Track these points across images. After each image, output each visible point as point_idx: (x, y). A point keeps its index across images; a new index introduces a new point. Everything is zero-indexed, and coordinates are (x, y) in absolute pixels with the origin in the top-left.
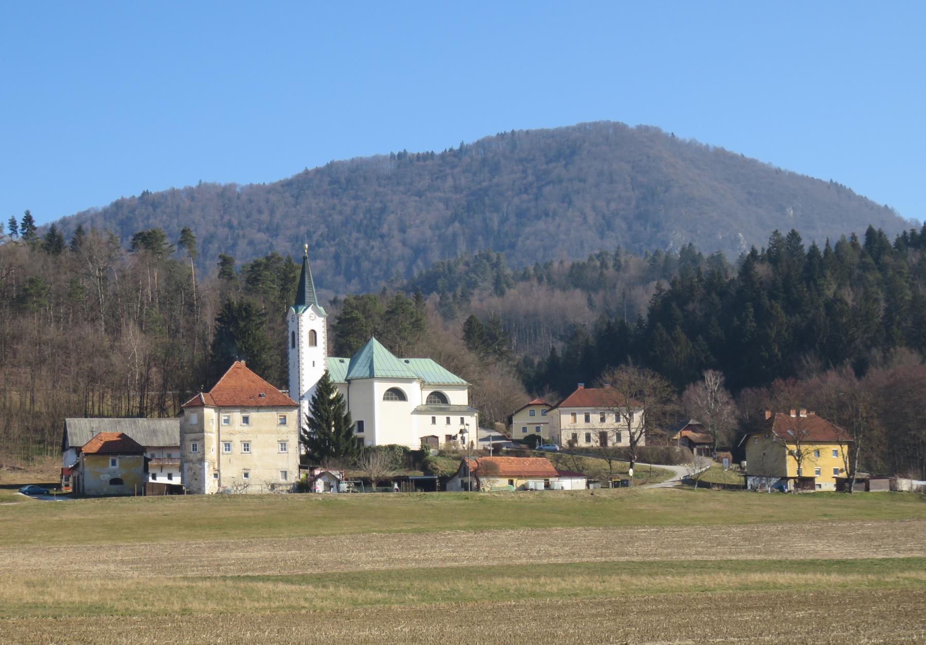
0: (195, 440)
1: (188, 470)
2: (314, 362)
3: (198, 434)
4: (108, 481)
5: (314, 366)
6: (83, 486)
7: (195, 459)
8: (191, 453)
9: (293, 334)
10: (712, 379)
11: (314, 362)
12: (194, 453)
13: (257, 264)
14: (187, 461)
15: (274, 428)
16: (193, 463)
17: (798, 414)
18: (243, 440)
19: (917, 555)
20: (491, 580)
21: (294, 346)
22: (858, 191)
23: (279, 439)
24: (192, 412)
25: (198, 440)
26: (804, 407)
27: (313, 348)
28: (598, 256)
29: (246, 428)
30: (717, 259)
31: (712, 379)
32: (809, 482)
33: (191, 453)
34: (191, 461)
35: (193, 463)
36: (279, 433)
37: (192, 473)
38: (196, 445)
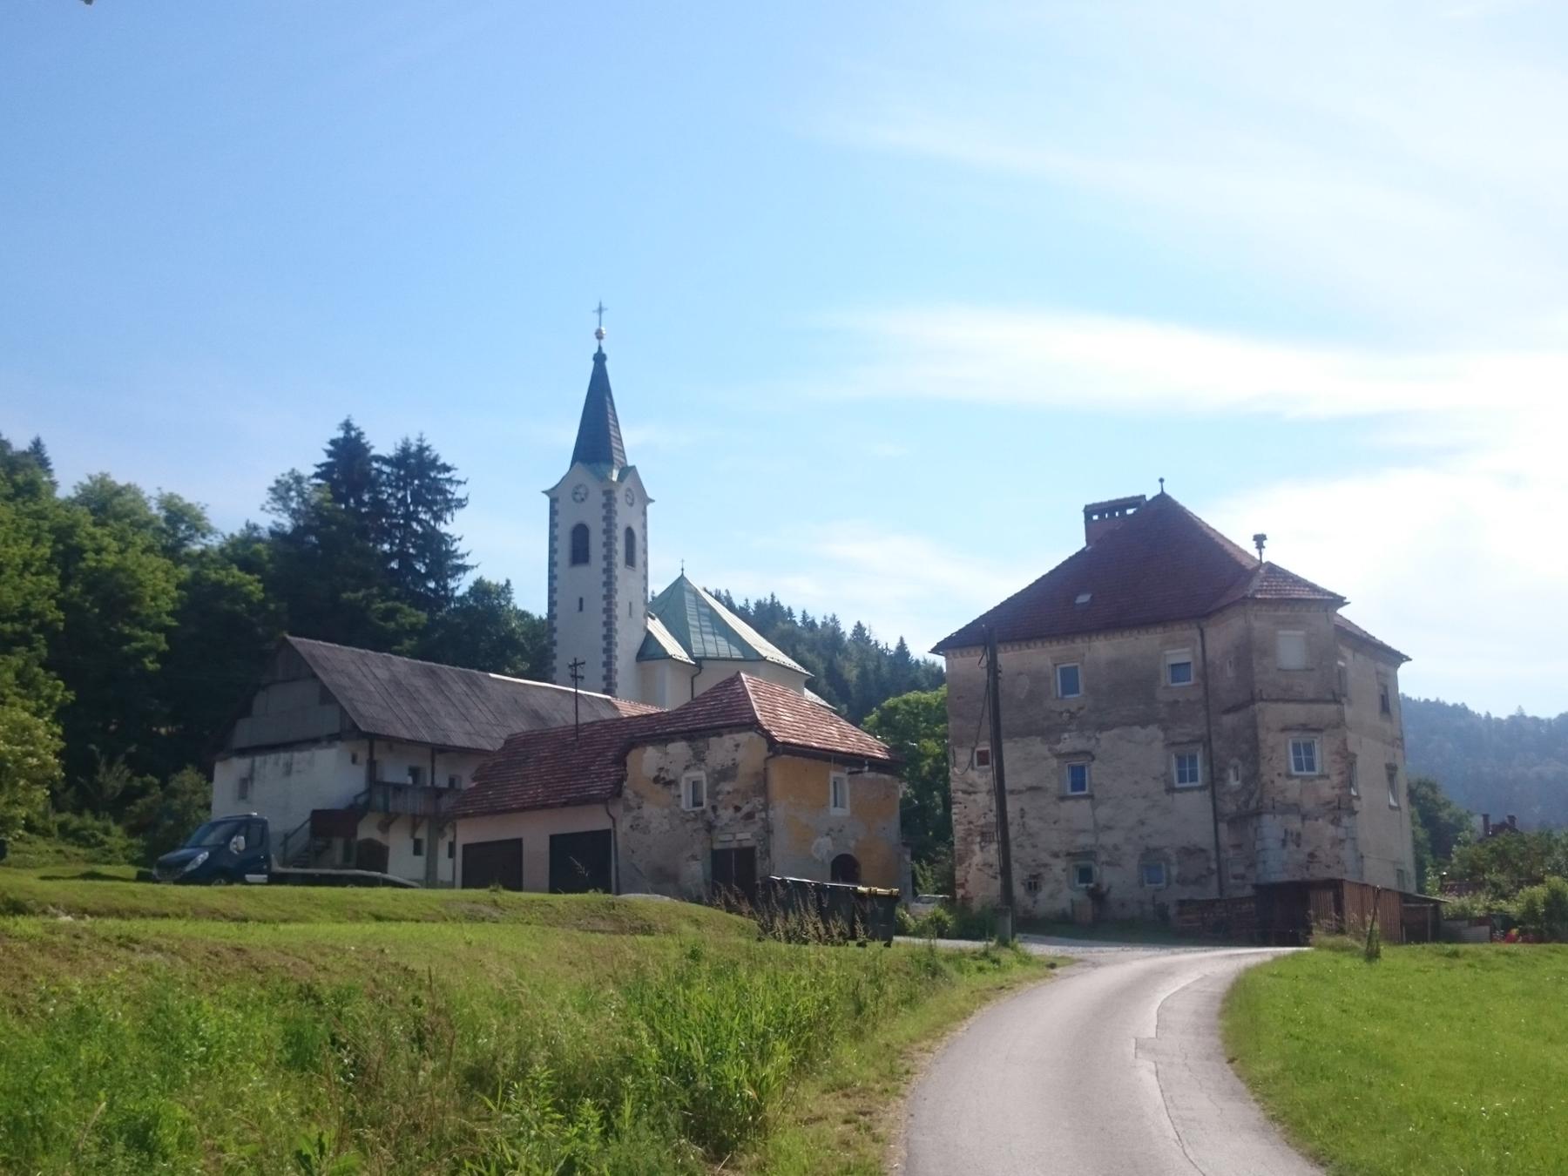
0: (1304, 728)
1: (1284, 843)
2: (581, 600)
3: (1317, 707)
4: (828, 862)
5: (581, 609)
7: (1309, 804)
8: (1289, 776)
9: (630, 533)
10: (15, 477)
11: (581, 600)
12: (1303, 778)
13: (218, 910)
16: (1304, 818)
17: (115, 724)
19: (325, 930)
20: (1489, 909)
21: (630, 560)
25: (1318, 730)
27: (581, 570)
28: (286, 1035)
31: (15, 477)
33: (1289, 776)
34: (1294, 808)
35: (1304, 818)
38: (1309, 749)
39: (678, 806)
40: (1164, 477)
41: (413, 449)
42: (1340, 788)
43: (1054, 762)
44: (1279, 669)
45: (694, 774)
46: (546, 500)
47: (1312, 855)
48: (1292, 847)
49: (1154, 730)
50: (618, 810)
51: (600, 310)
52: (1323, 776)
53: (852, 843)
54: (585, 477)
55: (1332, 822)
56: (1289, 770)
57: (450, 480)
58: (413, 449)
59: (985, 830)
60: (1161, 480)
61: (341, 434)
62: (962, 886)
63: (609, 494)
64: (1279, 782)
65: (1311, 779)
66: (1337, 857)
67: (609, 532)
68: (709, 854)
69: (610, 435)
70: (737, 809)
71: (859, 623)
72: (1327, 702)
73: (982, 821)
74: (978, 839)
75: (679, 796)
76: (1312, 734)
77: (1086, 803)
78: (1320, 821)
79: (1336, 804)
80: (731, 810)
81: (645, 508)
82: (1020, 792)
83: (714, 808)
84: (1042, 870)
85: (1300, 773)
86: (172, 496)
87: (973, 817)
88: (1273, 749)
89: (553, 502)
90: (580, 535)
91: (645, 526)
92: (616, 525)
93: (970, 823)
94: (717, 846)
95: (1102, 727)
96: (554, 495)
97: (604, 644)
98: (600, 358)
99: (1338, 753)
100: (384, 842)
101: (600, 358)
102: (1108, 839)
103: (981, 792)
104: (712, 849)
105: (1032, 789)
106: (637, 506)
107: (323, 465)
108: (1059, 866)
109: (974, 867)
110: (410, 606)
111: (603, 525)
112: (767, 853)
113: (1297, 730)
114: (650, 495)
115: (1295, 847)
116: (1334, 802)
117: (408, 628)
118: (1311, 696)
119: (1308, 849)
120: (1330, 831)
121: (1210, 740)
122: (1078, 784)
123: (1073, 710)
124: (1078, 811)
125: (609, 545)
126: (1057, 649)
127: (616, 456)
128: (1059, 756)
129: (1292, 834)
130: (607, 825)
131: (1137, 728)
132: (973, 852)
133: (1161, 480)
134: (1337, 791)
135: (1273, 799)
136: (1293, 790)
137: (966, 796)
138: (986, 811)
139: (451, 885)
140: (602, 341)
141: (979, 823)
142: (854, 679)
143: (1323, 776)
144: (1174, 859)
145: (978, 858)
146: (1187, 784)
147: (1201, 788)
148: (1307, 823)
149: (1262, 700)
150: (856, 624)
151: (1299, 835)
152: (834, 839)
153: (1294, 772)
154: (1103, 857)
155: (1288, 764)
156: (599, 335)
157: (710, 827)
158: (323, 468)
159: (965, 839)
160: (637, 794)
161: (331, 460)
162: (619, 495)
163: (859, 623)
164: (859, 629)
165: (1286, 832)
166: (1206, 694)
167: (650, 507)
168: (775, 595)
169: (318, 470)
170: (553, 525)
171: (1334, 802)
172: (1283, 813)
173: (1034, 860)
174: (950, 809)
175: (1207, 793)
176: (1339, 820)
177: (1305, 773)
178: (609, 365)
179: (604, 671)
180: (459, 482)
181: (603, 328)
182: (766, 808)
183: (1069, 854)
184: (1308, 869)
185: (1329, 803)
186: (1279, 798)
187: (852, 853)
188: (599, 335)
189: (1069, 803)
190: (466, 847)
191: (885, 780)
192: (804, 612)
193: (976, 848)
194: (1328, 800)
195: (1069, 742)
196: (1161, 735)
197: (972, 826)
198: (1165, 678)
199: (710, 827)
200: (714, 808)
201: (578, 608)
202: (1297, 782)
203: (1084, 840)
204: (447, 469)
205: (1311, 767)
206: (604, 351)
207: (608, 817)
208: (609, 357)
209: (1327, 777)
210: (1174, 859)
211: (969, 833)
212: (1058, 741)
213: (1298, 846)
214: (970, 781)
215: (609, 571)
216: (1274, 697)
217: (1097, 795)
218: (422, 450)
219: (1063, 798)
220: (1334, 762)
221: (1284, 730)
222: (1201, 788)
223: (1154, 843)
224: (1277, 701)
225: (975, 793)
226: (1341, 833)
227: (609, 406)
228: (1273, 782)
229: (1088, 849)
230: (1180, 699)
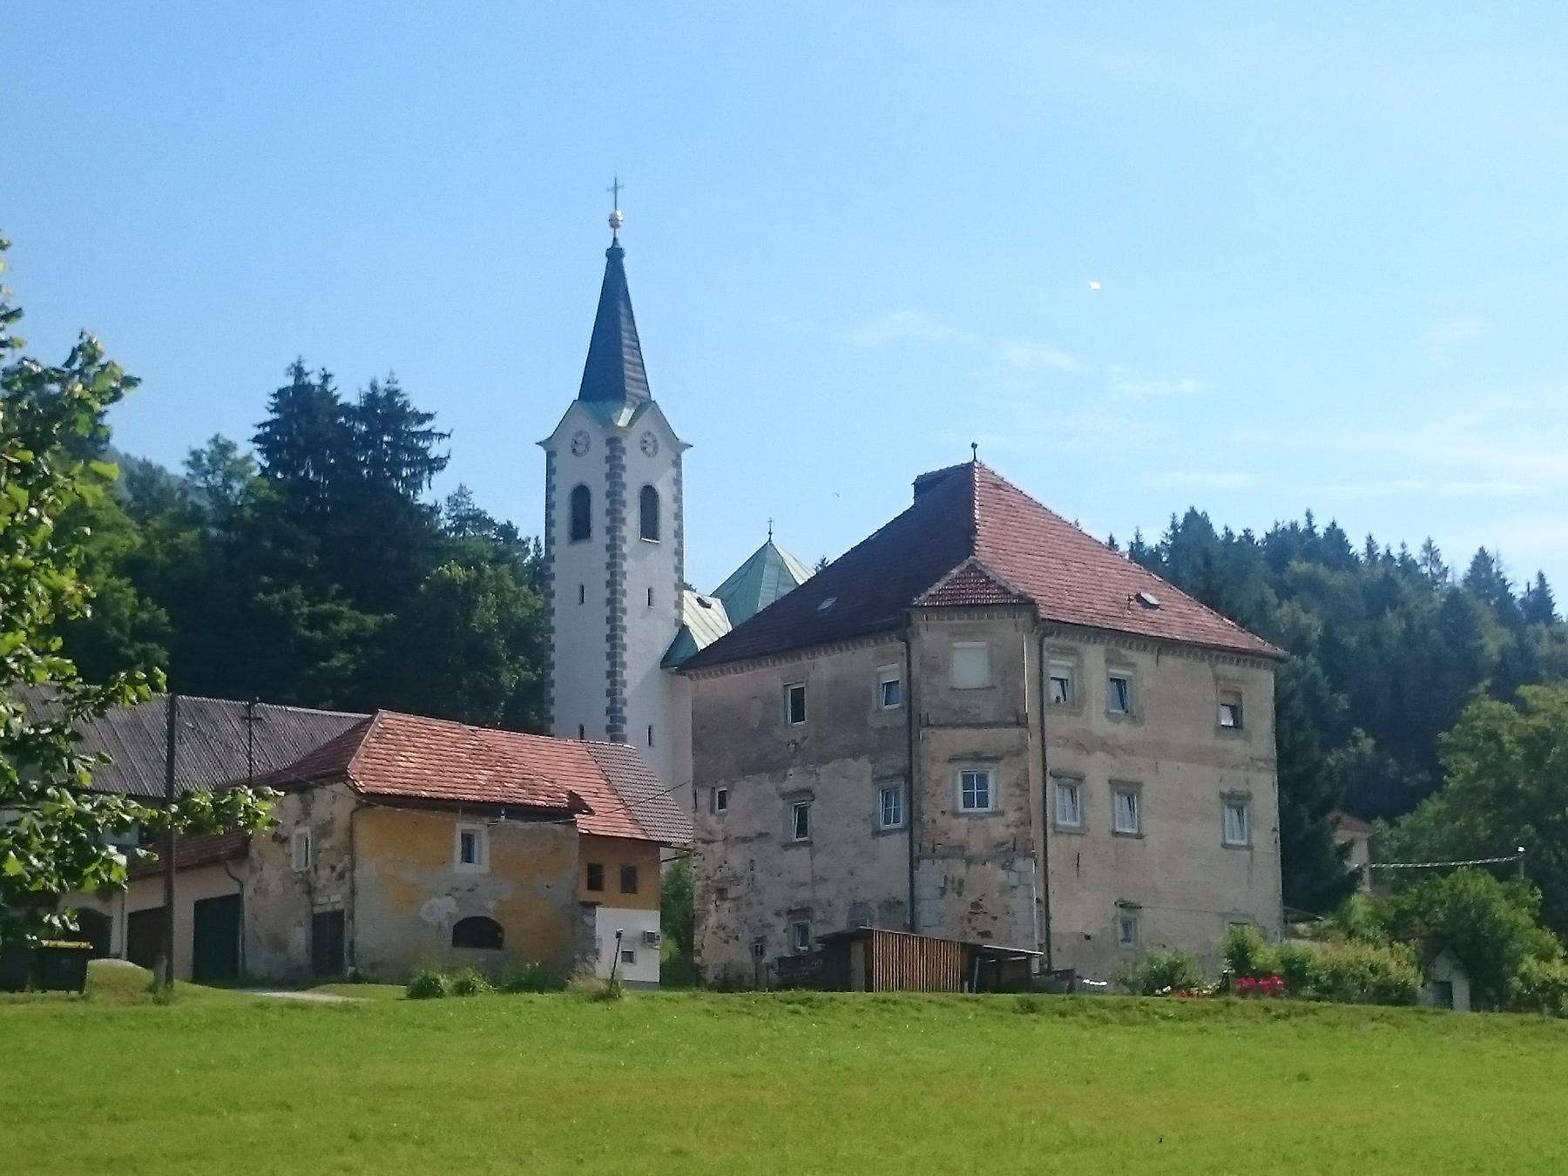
0: (978, 757)
1: (943, 891)
4: (448, 928)
6: (352, 943)
7: (976, 847)
8: (956, 814)
9: (649, 496)
14: (934, 854)
15: (1209, 739)
16: (969, 861)
18: (1116, 776)
21: (650, 529)
22: (1056, 511)
23: (1226, 790)
24: (957, 634)
26: (235, 815)
27: (581, 547)
29: (1123, 731)
30: (1247, 534)
32: (312, 885)
33: (956, 814)
34: (958, 852)
35: (969, 861)
36: (1221, 765)
37: (964, 908)
38: (983, 780)
39: (289, 865)
40: (976, 442)
41: (382, 394)
42: (1017, 827)
43: (780, 803)
44: (952, 689)
45: (301, 830)
46: (542, 454)
47: (976, 905)
48: (951, 896)
49: (863, 766)
50: (243, 873)
51: (616, 188)
52: (999, 813)
53: (491, 905)
54: (585, 423)
55: (1003, 867)
56: (955, 807)
57: (428, 435)
58: (382, 394)
59: (721, 885)
60: (974, 446)
61: (290, 381)
62: (699, 953)
63: (614, 443)
64: (942, 821)
65: (981, 817)
66: (1007, 906)
67: (614, 495)
68: (311, 917)
69: (622, 359)
70: (333, 868)
71: (1482, 550)
72: (1007, 725)
73: (718, 875)
74: (714, 897)
75: (291, 855)
76: (987, 764)
77: (805, 851)
78: (989, 864)
79: (1010, 845)
80: (328, 870)
81: (679, 456)
82: (751, 840)
83: (316, 867)
84: (766, 931)
85: (970, 810)
86: (146, 466)
87: (710, 871)
88: (938, 783)
89: (551, 455)
90: (581, 496)
91: (678, 482)
92: (624, 486)
93: (708, 878)
94: (317, 910)
95: (823, 760)
96: (550, 447)
97: (607, 647)
98: (615, 255)
99: (1018, 785)
100: (105, 912)
101: (615, 255)
102: (824, 893)
103: (718, 841)
104: (314, 915)
105: (761, 835)
106: (665, 454)
107: (264, 425)
108: (781, 924)
109: (709, 930)
110: (352, 607)
111: (606, 486)
112: (352, 917)
113: (967, 759)
114: (682, 436)
115: (956, 896)
116: (1007, 842)
117: (345, 637)
118: (989, 718)
119: (971, 899)
120: (1002, 875)
121: (911, 772)
122: (802, 829)
123: (798, 740)
124: (798, 859)
125: (614, 514)
126: (785, 666)
127: (630, 387)
128: (784, 796)
129: (953, 882)
130: (233, 889)
131: (850, 760)
132: (708, 912)
133: (974, 446)
134: (1013, 830)
135: (933, 842)
136: (958, 830)
137: (704, 846)
138: (722, 863)
139: (118, 957)
140: (617, 230)
141: (715, 878)
142: (1355, 645)
143: (999, 813)
144: (876, 914)
145: (712, 920)
146: (893, 826)
147: (900, 830)
148: (972, 867)
149: (928, 725)
150: (1476, 552)
151: (961, 883)
152: (458, 900)
153: (961, 809)
154: (819, 915)
155: (955, 799)
156: (614, 222)
157: (310, 891)
158: (268, 429)
159: (703, 898)
160: (260, 854)
161: (275, 416)
162: (631, 444)
163: (1482, 550)
164: (1482, 561)
165: (946, 879)
166: (910, 718)
167: (685, 455)
168: (1313, 513)
169: (260, 431)
170: (550, 488)
171: (1007, 842)
172: (944, 857)
173: (760, 921)
174: (940, 859)
175: (906, 835)
176: (1012, 862)
177: (976, 810)
178: (628, 263)
179: (607, 684)
180: (442, 435)
181: (619, 213)
182: (353, 868)
183: (790, 912)
184: (970, 921)
185: (1003, 844)
186: (942, 839)
187: (490, 915)
188: (614, 222)
189: (793, 852)
190: (130, 915)
191: (554, 831)
192: (1370, 538)
193: (712, 907)
194: (1001, 840)
195: (795, 779)
196: (870, 767)
197: (709, 882)
198: (877, 697)
199: (310, 891)
200: (316, 867)
201: (578, 600)
202: (964, 820)
203: (803, 895)
204: (422, 418)
205: (983, 803)
206: (622, 244)
207: (232, 880)
208: (627, 251)
209: (1002, 814)
210: (876, 914)
211: (707, 891)
212: (785, 778)
213: (960, 894)
214: (709, 828)
215: (612, 548)
216: (942, 722)
217: (815, 842)
218: (392, 394)
219: (787, 846)
220: (1011, 795)
221: (952, 760)
222: (900, 830)
223: (862, 895)
224: (944, 726)
225: (713, 842)
226: (1013, 879)
227: (623, 320)
228: (934, 821)
229: (806, 905)
230: (888, 725)
